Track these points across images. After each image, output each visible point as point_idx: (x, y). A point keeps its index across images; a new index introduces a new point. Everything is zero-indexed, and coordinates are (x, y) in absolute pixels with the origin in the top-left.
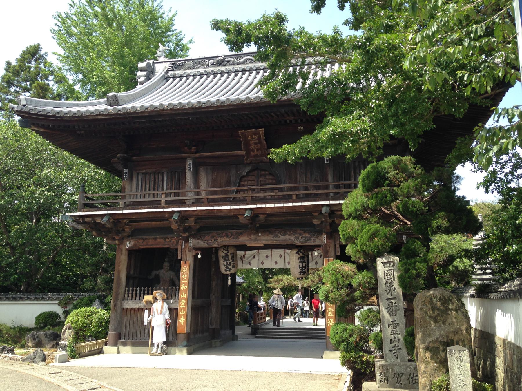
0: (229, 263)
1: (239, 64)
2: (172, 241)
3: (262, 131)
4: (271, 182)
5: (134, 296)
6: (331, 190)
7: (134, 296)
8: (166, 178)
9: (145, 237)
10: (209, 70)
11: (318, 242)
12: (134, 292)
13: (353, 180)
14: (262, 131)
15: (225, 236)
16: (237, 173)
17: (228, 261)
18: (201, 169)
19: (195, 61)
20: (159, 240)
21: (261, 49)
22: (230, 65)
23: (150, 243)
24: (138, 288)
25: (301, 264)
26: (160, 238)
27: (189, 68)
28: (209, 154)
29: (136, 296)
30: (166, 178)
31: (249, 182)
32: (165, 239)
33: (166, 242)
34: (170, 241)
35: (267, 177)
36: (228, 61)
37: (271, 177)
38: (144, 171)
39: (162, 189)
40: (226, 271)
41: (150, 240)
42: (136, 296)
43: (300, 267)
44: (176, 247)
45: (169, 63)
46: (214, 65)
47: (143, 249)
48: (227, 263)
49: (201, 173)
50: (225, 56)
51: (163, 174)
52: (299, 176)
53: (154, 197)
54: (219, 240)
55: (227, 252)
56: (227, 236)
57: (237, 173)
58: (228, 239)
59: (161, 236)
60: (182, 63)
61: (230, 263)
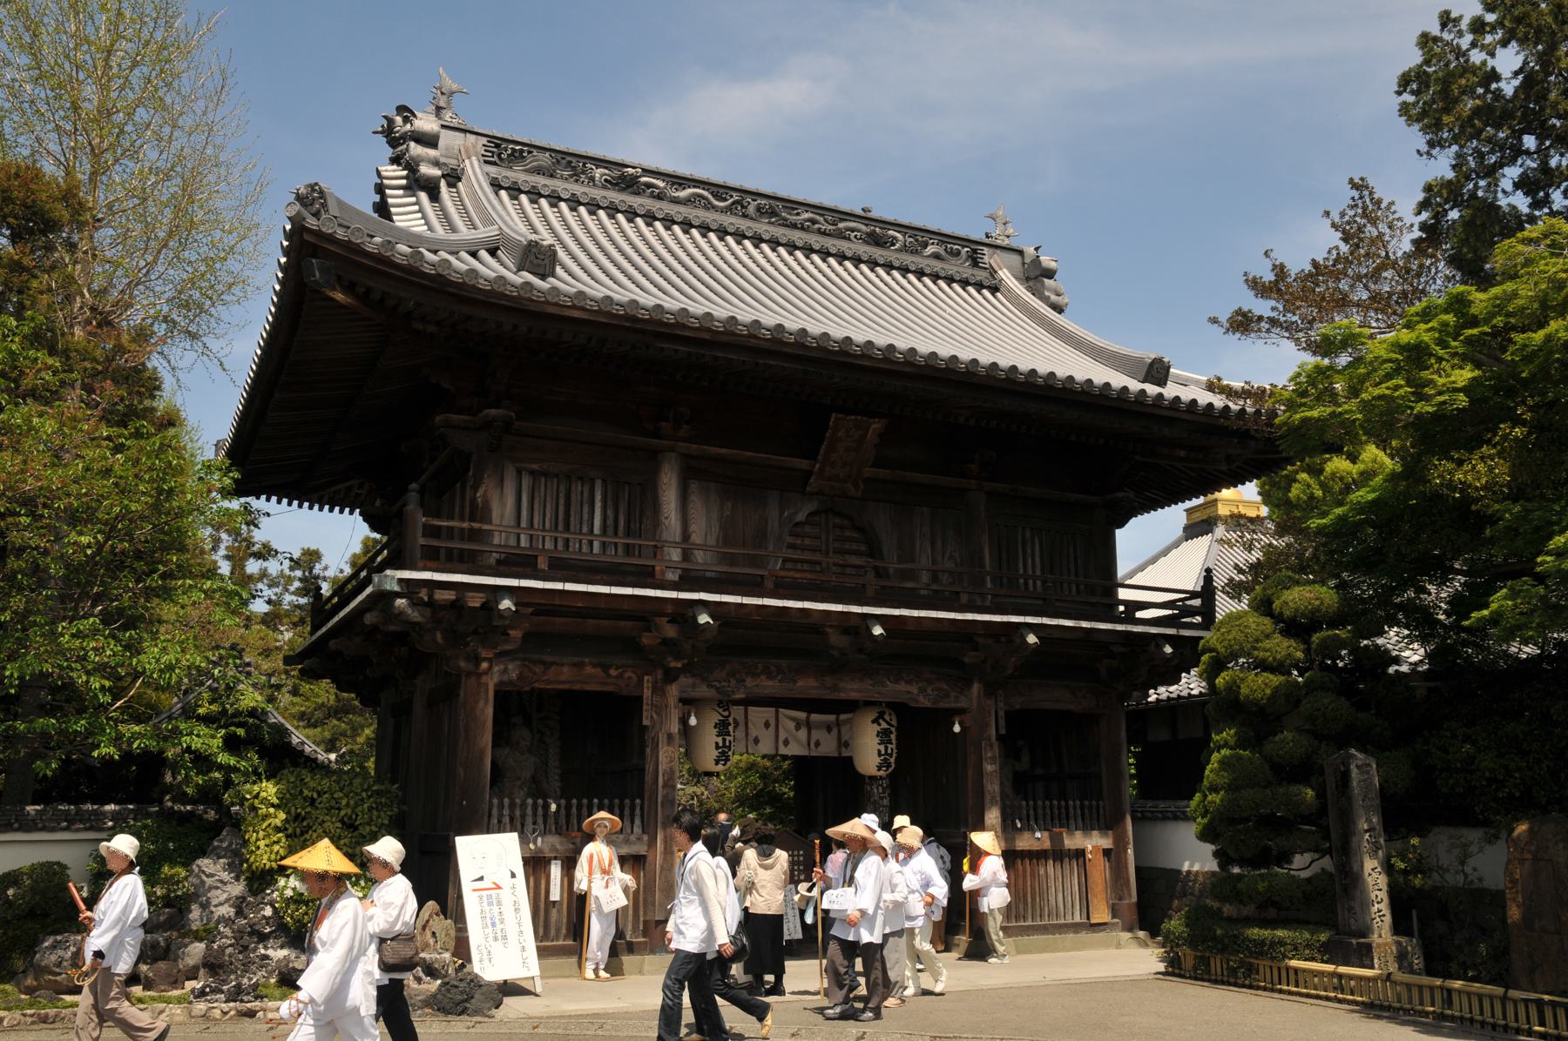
1: (676, 201)
2: (627, 675)
3: (876, 425)
4: (855, 547)
8: (598, 497)
9: (549, 659)
10: (597, 194)
11: (963, 704)
14: (876, 425)
16: (781, 514)
18: (694, 486)
19: (966, 271)
20: (589, 670)
21: (1527, 416)
22: (652, 196)
23: (563, 678)
24: (585, 801)
25: (882, 748)
26: (595, 666)
27: (538, 171)
28: (724, 451)
30: (598, 497)
31: (807, 542)
32: (605, 668)
33: (609, 676)
34: (621, 676)
35: (847, 533)
36: (649, 186)
37: (855, 535)
38: (535, 467)
41: (565, 669)
43: (880, 754)
45: (484, 140)
46: (611, 184)
49: (692, 498)
50: (644, 170)
52: (918, 543)
54: (749, 682)
57: (781, 514)
58: (770, 683)
60: (521, 151)
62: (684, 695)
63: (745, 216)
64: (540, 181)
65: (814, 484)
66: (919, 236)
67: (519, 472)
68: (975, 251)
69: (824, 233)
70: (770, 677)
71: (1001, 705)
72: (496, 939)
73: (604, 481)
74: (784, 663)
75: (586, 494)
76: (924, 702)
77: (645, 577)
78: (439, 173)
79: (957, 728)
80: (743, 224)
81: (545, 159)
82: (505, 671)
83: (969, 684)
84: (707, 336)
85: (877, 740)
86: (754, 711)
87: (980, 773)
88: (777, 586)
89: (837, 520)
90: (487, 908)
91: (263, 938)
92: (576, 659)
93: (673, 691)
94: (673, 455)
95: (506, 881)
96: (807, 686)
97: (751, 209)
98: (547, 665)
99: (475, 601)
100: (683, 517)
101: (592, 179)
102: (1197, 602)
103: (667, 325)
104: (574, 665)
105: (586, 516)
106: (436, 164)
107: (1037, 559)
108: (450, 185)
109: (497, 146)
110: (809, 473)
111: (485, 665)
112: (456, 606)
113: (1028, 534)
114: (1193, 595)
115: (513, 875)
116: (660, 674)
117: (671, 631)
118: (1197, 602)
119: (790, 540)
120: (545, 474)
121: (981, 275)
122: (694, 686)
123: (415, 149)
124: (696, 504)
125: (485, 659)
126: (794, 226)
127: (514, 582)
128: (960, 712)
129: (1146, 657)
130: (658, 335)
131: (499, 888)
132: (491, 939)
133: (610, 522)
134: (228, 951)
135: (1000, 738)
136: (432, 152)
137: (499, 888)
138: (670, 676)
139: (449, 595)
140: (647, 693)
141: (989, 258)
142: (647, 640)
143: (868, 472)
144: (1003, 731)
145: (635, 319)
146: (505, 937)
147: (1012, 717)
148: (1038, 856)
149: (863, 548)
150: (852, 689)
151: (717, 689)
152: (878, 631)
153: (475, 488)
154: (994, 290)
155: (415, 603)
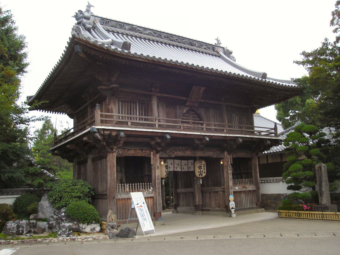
0: (201, 171)
1: (145, 34)
3: (203, 89)
5: (134, 189)
6: (157, 123)
7: (134, 189)
10: (127, 32)
11: (223, 156)
12: (139, 186)
13: (233, 124)
15: (178, 151)
17: (201, 170)
19: (213, 52)
20: (138, 151)
24: (131, 184)
26: (139, 150)
27: (112, 26)
29: (132, 189)
32: (142, 150)
33: (143, 152)
34: (145, 152)
35: (195, 116)
36: (139, 30)
37: (197, 116)
38: (123, 100)
39: (136, 115)
40: (200, 175)
42: (147, 189)
44: (149, 156)
45: (100, 19)
47: (132, 156)
48: (200, 170)
51: (136, 103)
52: (211, 118)
53: (140, 120)
54: (175, 153)
55: (201, 163)
56: (179, 150)
58: (180, 153)
59: (139, 148)
60: (108, 21)
61: (202, 171)
62: (161, 157)
63: (161, 38)
64: (113, 29)
65: (188, 104)
66: (201, 44)
67: (119, 101)
68: (213, 48)
69: (180, 43)
70: (180, 151)
71: (231, 157)
72: (144, 220)
73: (139, 103)
74: (183, 148)
75: (135, 106)
76: (215, 156)
77: (152, 126)
78: (91, 26)
79: (222, 163)
80: (161, 40)
81: (114, 23)
82: (119, 152)
83: (224, 152)
84: (171, 66)
85: (165, 168)
86: (176, 161)
87: (228, 173)
88: (184, 128)
89: (192, 112)
90: (141, 212)
91: (63, 221)
92: (135, 148)
93: (158, 155)
94: (155, 96)
95: (143, 205)
96: (188, 153)
97: (163, 36)
98: (128, 150)
99: (114, 134)
100: (158, 113)
101: (125, 28)
102: (273, 131)
103: (161, 62)
104: (135, 150)
105: (135, 112)
106: (90, 24)
107: (237, 121)
108: (93, 30)
109: (103, 20)
110: (186, 101)
111: (115, 150)
112: (110, 135)
113: (235, 115)
114: (272, 129)
115: (144, 203)
116: (155, 151)
117: (159, 140)
118: (273, 131)
119: (182, 117)
120: (125, 102)
121: (215, 53)
122: (162, 154)
123: (85, 21)
124: (160, 108)
125: (115, 149)
126: (173, 41)
127: (124, 129)
128: (222, 158)
129: (262, 144)
130: (158, 65)
131: (142, 206)
132: (143, 220)
133: (141, 113)
134: (54, 224)
135: (231, 164)
136: (89, 21)
137: (142, 206)
138: (157, 152)
139: (108, 132)
140: (152, 156)
141: (216, 49)
142: (153, 143)
143: (200, 100)
144: (232, 163)
145: (154, 61)
146: (146, 220)
147: (234, 159)
148: (240, 192)
149: (198, 119)
150: (199, 154)
151: (168, 155)
152: (208, 139)
153: (109, 105)
154: (219, 57)
155: (101, 135)
